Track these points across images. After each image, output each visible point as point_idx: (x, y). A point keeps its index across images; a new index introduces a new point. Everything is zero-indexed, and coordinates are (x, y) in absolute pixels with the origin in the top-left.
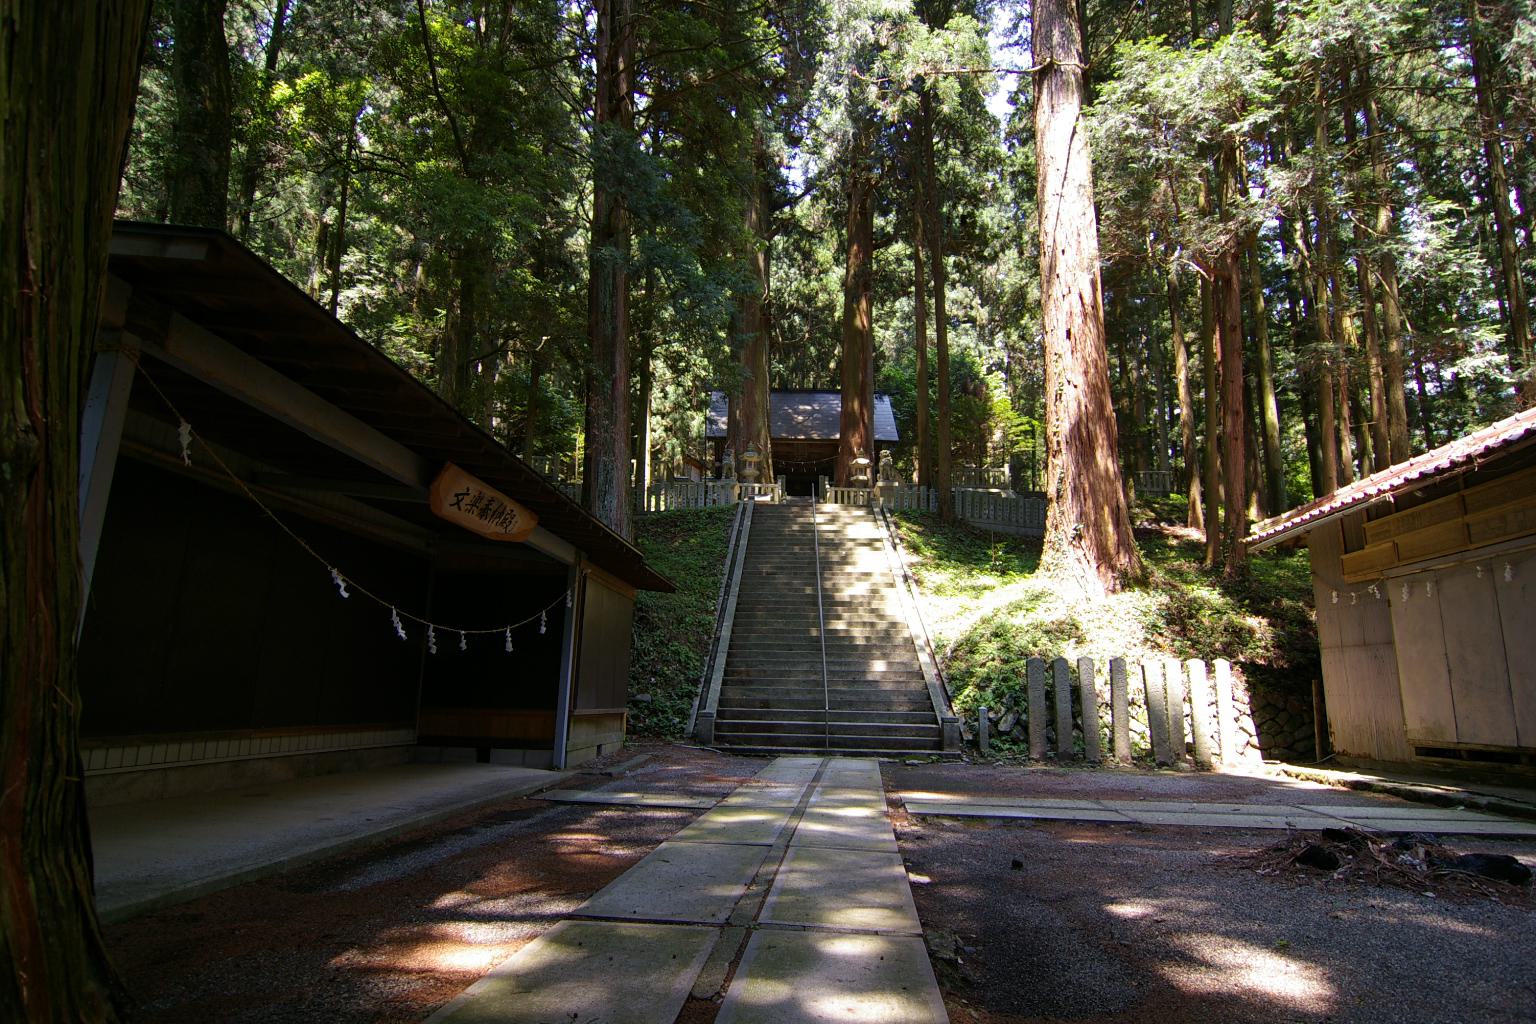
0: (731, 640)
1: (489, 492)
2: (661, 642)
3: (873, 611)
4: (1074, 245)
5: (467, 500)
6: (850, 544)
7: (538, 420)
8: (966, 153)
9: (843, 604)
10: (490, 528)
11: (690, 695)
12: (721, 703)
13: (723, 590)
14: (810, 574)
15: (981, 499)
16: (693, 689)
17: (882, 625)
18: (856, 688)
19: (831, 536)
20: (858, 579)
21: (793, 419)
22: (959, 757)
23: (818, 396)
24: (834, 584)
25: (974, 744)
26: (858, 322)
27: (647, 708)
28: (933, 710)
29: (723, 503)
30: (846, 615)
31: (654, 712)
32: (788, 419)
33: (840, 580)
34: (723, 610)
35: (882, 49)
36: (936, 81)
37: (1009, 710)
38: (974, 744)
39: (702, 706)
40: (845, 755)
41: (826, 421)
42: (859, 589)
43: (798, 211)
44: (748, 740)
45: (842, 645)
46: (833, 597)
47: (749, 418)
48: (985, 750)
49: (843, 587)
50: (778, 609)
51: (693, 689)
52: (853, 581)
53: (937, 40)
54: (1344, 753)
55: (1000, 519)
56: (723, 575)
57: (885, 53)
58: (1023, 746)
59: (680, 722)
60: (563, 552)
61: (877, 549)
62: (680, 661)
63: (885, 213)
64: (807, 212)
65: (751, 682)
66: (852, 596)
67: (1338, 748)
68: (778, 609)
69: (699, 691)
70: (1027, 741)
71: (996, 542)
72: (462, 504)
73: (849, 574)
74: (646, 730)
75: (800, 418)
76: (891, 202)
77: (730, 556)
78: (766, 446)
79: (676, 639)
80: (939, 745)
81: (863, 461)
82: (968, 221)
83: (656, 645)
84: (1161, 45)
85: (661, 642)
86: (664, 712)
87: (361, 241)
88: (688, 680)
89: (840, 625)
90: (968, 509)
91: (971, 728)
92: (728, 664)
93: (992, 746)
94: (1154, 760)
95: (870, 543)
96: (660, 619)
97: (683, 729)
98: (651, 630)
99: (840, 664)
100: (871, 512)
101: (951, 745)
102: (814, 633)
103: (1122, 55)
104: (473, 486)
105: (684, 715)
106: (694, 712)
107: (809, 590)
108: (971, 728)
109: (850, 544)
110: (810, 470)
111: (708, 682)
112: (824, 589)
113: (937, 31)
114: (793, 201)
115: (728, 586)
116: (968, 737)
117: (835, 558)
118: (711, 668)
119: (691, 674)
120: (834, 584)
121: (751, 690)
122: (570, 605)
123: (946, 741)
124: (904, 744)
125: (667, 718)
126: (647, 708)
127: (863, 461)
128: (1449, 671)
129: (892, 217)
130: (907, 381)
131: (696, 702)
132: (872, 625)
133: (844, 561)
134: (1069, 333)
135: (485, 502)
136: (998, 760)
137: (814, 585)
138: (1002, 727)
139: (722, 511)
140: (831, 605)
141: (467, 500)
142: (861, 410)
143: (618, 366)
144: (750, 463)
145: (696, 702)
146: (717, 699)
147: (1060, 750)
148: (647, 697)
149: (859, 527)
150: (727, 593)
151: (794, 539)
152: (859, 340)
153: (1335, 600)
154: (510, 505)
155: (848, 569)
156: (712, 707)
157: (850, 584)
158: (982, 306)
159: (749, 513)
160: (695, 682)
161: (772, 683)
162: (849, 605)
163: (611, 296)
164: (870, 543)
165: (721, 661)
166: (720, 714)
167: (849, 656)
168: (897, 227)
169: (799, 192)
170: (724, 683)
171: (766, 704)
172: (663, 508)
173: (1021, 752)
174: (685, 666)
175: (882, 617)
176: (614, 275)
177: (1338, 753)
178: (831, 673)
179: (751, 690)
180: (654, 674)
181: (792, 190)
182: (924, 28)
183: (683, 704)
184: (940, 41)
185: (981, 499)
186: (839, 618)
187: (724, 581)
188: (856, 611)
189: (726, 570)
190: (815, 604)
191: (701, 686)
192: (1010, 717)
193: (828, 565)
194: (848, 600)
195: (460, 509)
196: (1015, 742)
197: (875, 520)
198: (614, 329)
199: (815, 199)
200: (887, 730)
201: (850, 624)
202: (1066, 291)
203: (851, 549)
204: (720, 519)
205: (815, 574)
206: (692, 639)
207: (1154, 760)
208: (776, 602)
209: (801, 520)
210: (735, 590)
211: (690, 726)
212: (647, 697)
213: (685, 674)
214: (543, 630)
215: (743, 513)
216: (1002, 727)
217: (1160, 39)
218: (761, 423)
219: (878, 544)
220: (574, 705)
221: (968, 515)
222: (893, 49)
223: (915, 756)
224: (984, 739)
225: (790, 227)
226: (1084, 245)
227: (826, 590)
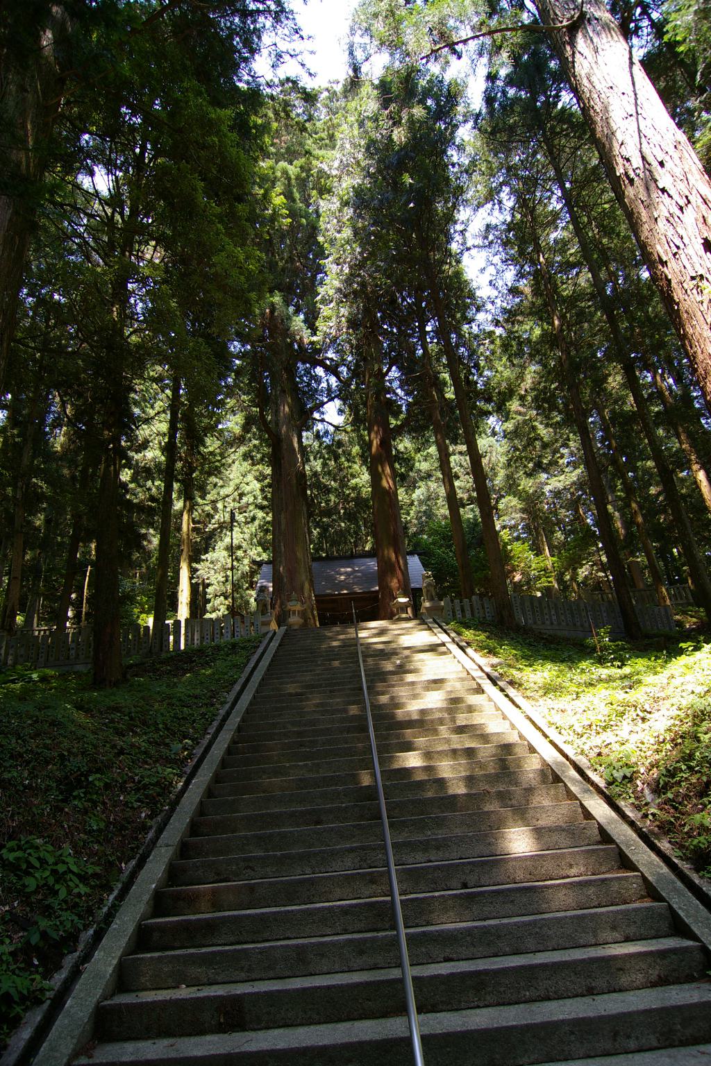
3: (461, 730)
6: (407, 652)
9: (410, 724)
14: (354, 689)
15: (540, 604)
17: (486, 752)
19: (380, 647)
20: (427, 689)
21: (336, 579)
23: (356, 561)
24: (392, 698)
26: (385, 484)
30: (421, 741)
32: (331, 579)
33: (402, 692)
41: (367, 577)
42: (433, 700)
45: (420, 802)
46: (393, 716)
47: (292, 573)
49: (404, 700)
52: (419, 690)
55: (564, 624)
56: (223, 703)
61: (444, 653)
66: (423, 712)
71: (597, 627)
73: (413, 683)
75: (343, 577)
78: (310, 597)
81: (403, 600)
89: (413, 760)
95: (433, 648)
99: (425, 846)
100: (423, 622)
102: (366, 780)
107: (354, 710)
109: (407, 652)
112: (377, 707)
117: (389, 666)
120: (392, 698)
127: (403, 600)
130: (431, 544)
132: (470, 752)
133: (402, 670)
137: (361, 702)
140: (394, 730)
142: (397, 558)
144: (294, 612)
149: (413, 636)
151: (332, 654)
152: (387, 499)
155: (410, 678)
157: (415, 697)
162: (423, 722)
164: (433, 648)
167: (440, 823)
172: (182, 647)
175: (485, 738)
178: (412, 877)
185: (540, 604)
186: (408, 747)
187: (222, 712)
188: (435, 732)
189: (231, 697)
190: (365, 729)
193: (379, 677)
194: (415, 717)
197: (430, 629)
201: (428, 755)
202: (682, 202)
203: (407, 657)
205: (361, 689)
208: (300, 734)
209: (342, 637)
215: (271, 639)
218: (303, 577)
219: (443, 649)
221: (530, 621)
227: (380, 707)
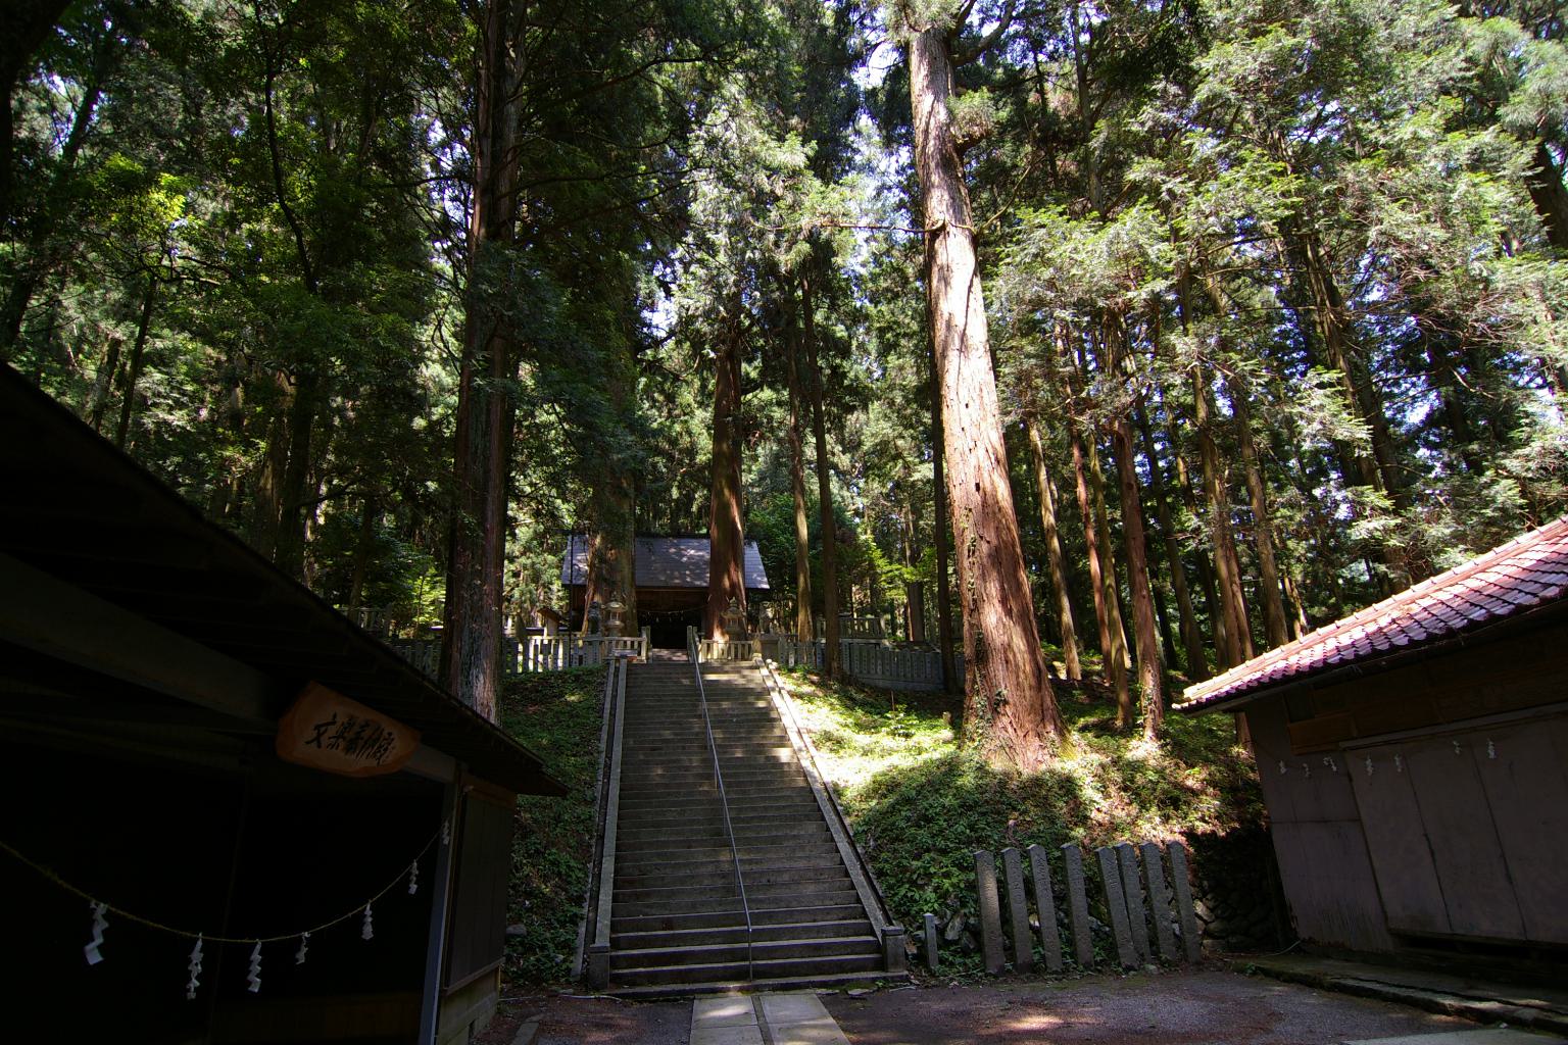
0: (618, 839)
1: (363, 714)
2: (537, 851)
4: (978, 402)
5: (332, 730)
7: (369, 566)
8: (833, 307)
10: (359, 763)
11: (574, 920)
12: (614, 927)
13: (601, 772)
16: (575, 910)
18: (772, 894)
22: (907, 979)
25: (921, 959)
27: (521, 943)
28: (867, 917)
29: (590, 662)
31: (530, 950)
34: (605, 797)
35: (777, 199)
36: (832, 234)
37: (955, 912)
38: (921, 959)
39: (591, 935)
40: (775, 988)
43: (662, 354)
44: (653, 979)
48: (936, 967)
50: (669, 794)
51: (575, 910)
53: (832, 195)
54: (1311, 940)
57: (782, 204)
58: (977, 959)
59: (564, 961)
60: (438, 768)
62: (559, 874)
63: (750, 361)
64: (672, 354)
65: (648, 895)
67: (1303, 934)
68: (669, 794)
69: (585, 911)
70: (980, 949)
72: (324, 740)
74: (521, 976)
76: (756, 349)
77: (605, 728)
79: (554, 845)
80: (881, 965)
82: (838, 374)
83: (530, 856)
84: (1061, 214)
85: (537, 851)
86: (543, 948)
87: (162, 360)
88: (570, 899)
90: (856, 663)
91: (915, 939)
92: (616, 872)
93: (942, 961)
94: (1119, 964)
96: (535, 821)
97: (569, 970)
98: (524, 837)
101: (896, 964)
103: (1021, 220)
104: (338, 710)
105: (568, 947)
106: (580, 942)
108: (915, 939)
110: (674, 617)
111: (595, 898)
113: (832, 185)
114: (658, 343)
115: (608, 767)
116: (913, 950)
118: (598, 877)
119: (574, 890)
121: (648, 906)
122: (446, 842)
123: (890, 960)
124: (841, 967)
125: (547, 956)
126: (521, 943)
128: (1433, 854)
129: (758, 363)
130: (774, 526)
131: (582, 930)
134: (977, 485)
135: (356, 728)
136: (952, 980)
138: (951, 935)
139: (591, 672)
141: (332, 730)
143: (490, 514)
145: (582, 930)
146: (608, 922)
147: (1019, 961)
148: (521, 929)
150: (607, 776)
153: (1283, 770)
154: (388, 726)
156: (602, 941)
158: (844, 453)
159: (622, 676)
160: (578, 901)
161: (673, 893)
163: (485, 434)
165: (608, 865)
166: (615, 944)
168: (762, 373)
169: (663, 334)
170: (615, 899)
171: (668, 924)
173: (976, 966)
174: (564, 881)
176: (488, 410)
177: (1303, 941)
179: (648, 906)
180: (529, 895)
181: (655, 332)
182: (817, 183)
183: (563, 935)
184: (836, 196)
187: (602, 759)
189: (603, 746)
191: (586, 905)
192: (957, 922)
195: (319, 746)
196: (965, 953)
198: (487, 472)
199: (679, 343)
200: (817, 949)
202: (972, 445)
204: (589, 682)
206: (572, 842)
207: (1119, 964)
210: (616, 771)
211: (577, 964)
212: (521, 929)
213: (566, 890)
214: (414, 888)
215: (616, 675)
216: (951, 935)
217: (1060, 209)
220: (446, 981)
222: (789, 199)
223: (857, 983)
224: (934, 953)
225: (655, 367)
226: (986, 400)
